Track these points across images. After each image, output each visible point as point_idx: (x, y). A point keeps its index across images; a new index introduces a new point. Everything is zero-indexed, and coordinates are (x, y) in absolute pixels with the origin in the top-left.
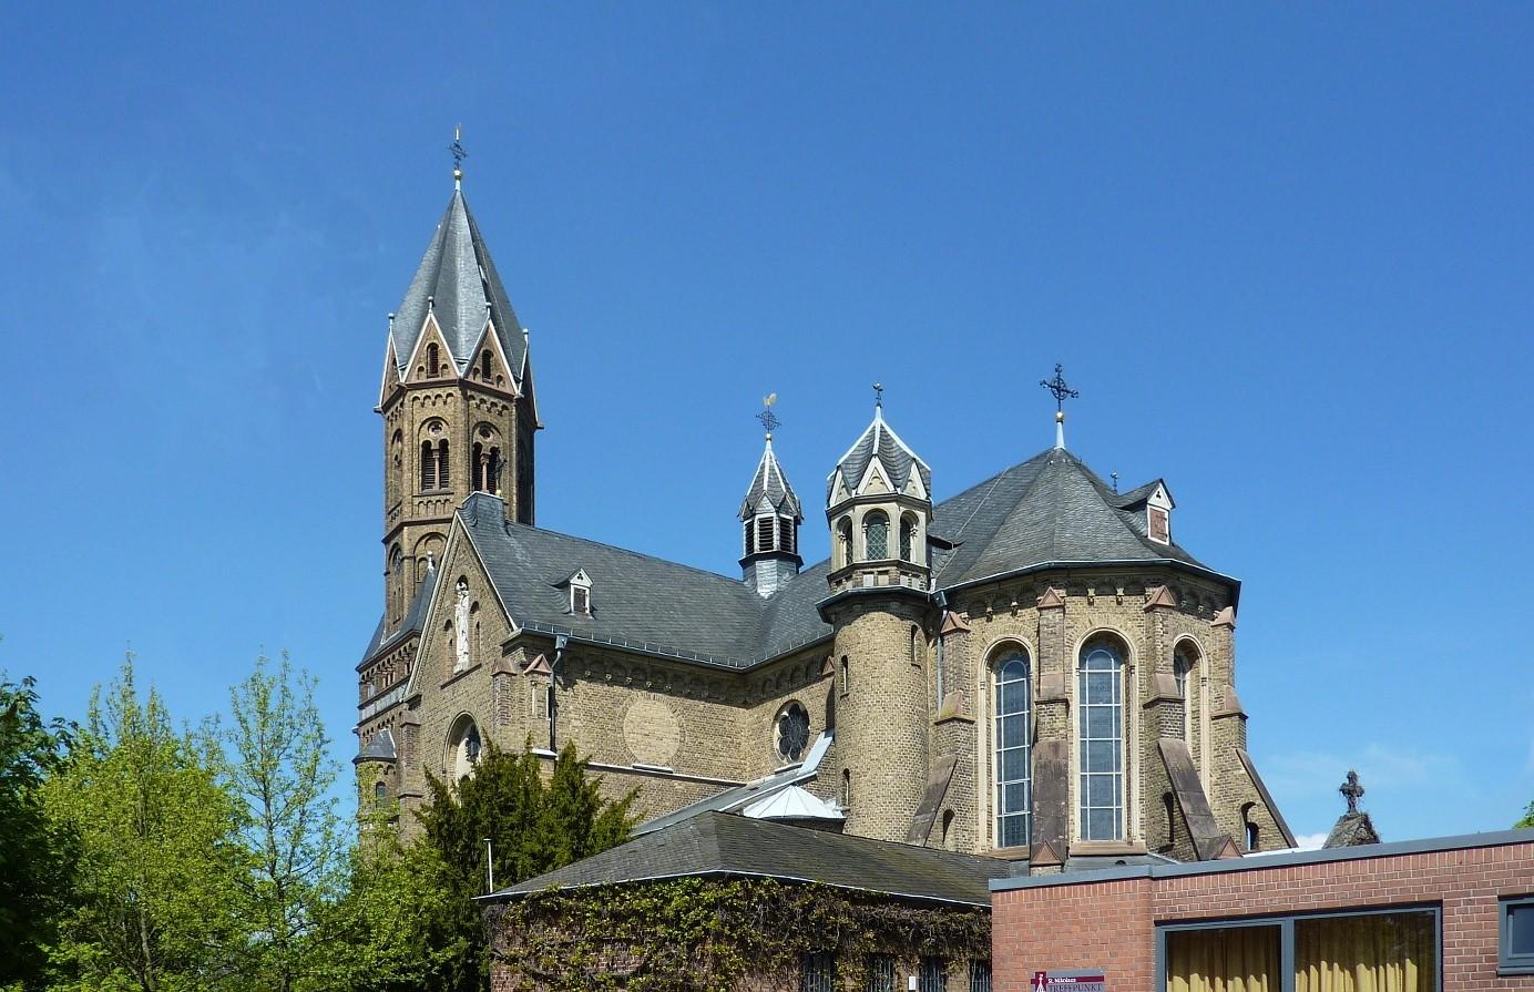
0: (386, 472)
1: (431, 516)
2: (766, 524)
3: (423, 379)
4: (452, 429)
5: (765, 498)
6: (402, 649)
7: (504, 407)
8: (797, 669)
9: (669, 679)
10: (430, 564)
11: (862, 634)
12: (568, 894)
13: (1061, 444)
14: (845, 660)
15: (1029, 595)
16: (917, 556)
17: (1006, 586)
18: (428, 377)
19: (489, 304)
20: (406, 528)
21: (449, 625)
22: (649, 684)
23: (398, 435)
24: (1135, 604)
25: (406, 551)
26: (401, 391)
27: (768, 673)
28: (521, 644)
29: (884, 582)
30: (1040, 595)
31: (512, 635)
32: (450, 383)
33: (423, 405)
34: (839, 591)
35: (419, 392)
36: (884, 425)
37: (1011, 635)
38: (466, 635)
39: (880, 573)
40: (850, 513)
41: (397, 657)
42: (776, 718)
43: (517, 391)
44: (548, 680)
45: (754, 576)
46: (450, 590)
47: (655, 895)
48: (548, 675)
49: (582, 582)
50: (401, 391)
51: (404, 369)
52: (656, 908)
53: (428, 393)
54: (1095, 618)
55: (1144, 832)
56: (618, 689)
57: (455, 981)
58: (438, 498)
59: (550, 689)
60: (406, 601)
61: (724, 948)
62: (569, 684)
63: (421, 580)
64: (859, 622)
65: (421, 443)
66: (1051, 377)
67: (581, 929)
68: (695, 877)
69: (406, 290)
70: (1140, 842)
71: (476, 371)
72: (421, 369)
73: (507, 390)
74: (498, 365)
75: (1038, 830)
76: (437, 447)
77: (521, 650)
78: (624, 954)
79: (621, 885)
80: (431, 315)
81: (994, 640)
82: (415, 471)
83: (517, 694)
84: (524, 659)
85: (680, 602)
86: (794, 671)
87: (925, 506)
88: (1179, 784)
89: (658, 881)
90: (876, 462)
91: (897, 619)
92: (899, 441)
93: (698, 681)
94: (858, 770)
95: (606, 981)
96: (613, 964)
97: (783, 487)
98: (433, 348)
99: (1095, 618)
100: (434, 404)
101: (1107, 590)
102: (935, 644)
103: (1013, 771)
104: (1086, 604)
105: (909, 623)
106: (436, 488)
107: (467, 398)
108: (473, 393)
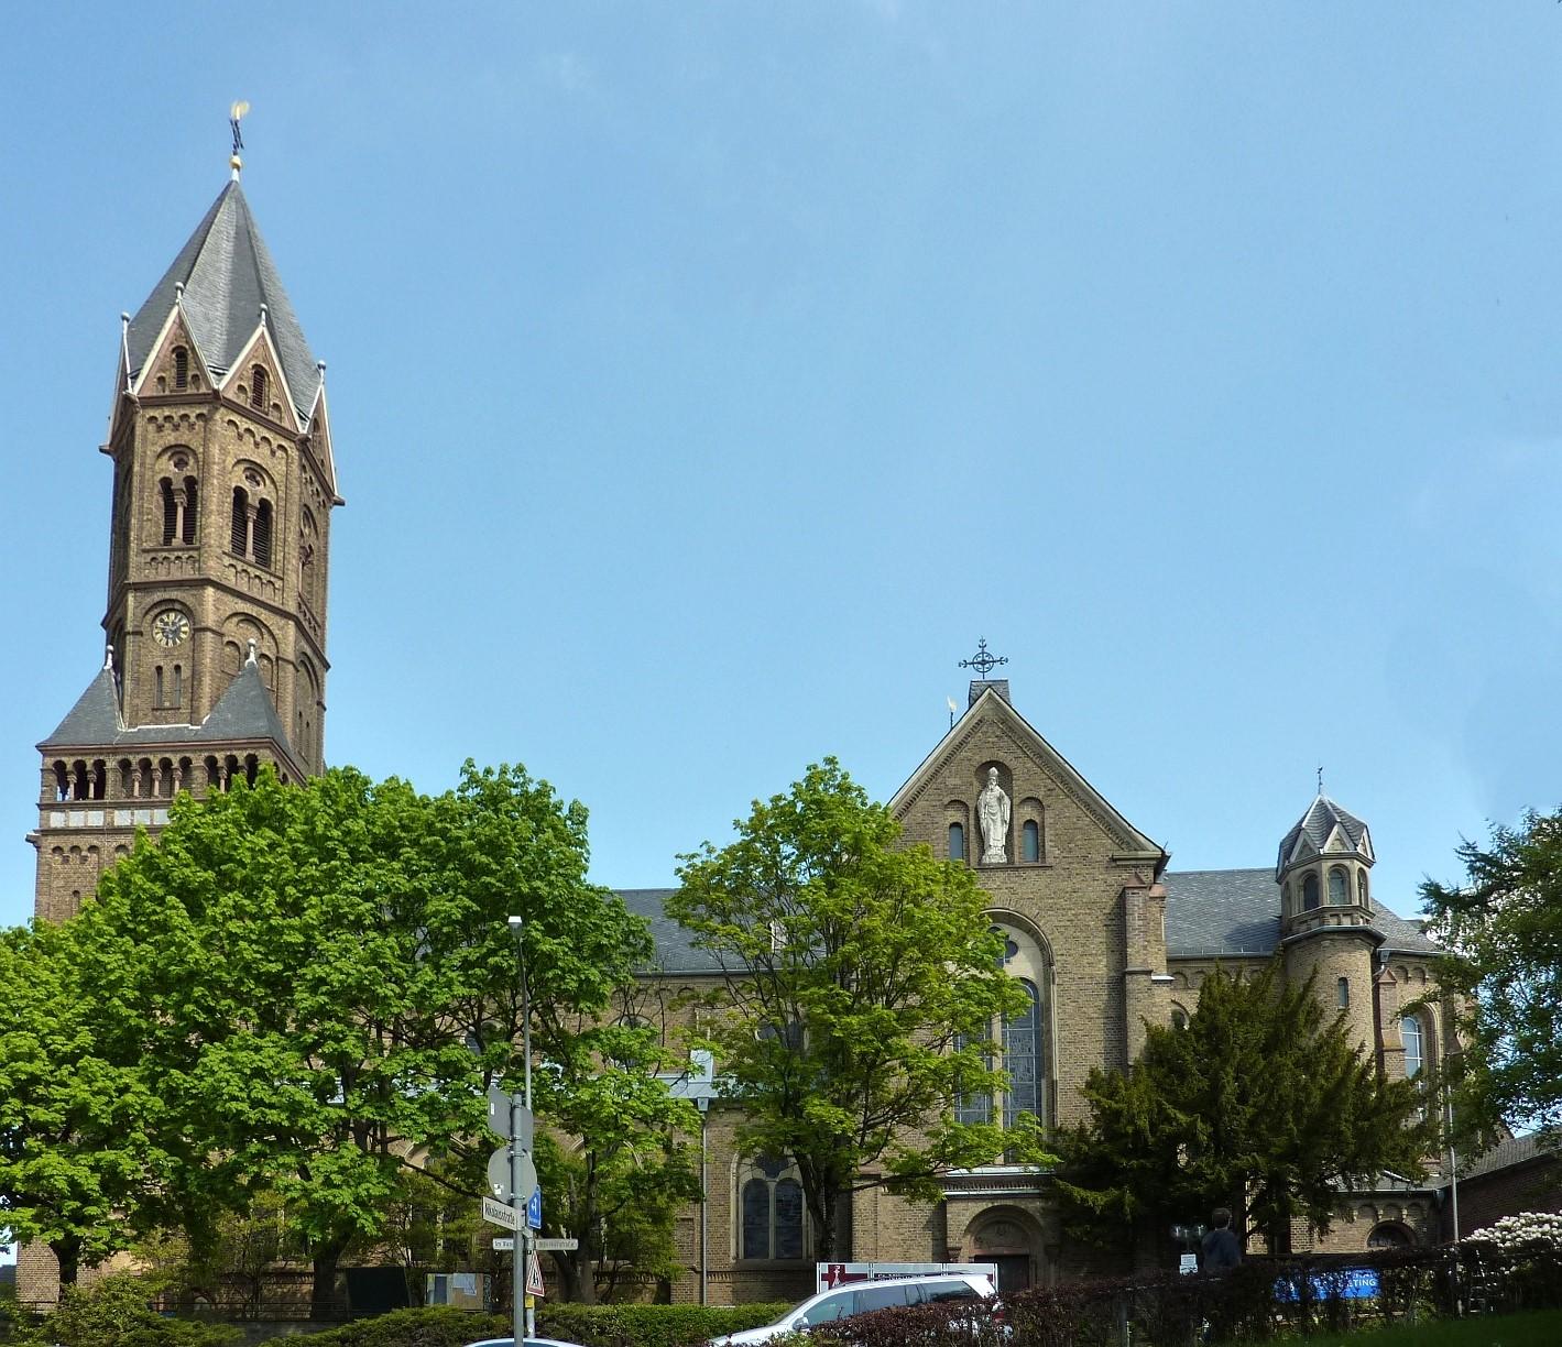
98: (260, 374)
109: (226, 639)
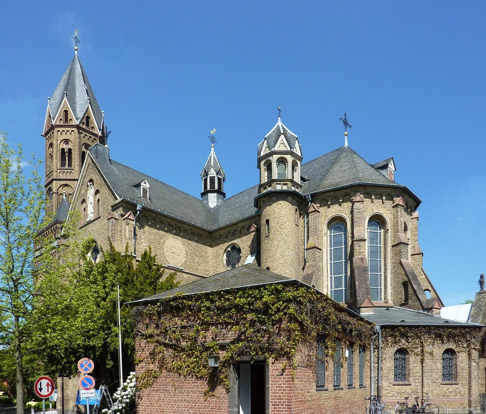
0: (46, 160)
1: (64, 177)
2: (212, 179)
3: (62, 123)
4: (73, 144)
5: (212, 168)
6: (52, 228)
7: (94, 139)
8: (236, 230)
9: (182, 231)
10: (64, 196)
11: (276, 210)
12: (189, 298)
13: (346, 144)
14: (268, 221)
15: (347, 197)
16: (297, 179)
17: (337, 193)
18: (64, 123)
19: (89, 98)
20: (54, 181)
21: (84, 201)
22: (174, 232)
23: (51, 145)
24: (389, 204)
25: (54, 190)
26: (53, 127)
27: (222, 232)
28: (121, 206)
29: (285, 188)
30: (352, 197)
31: (117, 202)
32: (73, 126)
33: (61, 134)
34: (265, 191)
35: (60, 128)
36: (282, 125)
37: (339, 213)
38: (92, 205)
39: (284, 184)
40: (271, 158)
41: (50, 232)
42: (225, 251)
43: (100, 134)
44: (134, 223)
45: (207, 199)
46: (85, 186)
47: (250, 296)
48: (133, 220)
49: (145, 185)
50: (53, 127)
51: (54, 119)
52: (249, 304)
53: (64, 129)
54: (374, 208)
55: (392, 298)
56: (161, 232)
57: (97, 354)
58: (67, 171)
59: (134, 227)
60: (54, 210)
61: (293, 326)
62: (141, 227)
63: (60, 202)
64: (274, 205)
65: (61, 149)
66: (343, 118)
67: (195, 318)
68: (278, 284)
69: (55, 88)
70: (390, 303)
71: (83, 123)
72: (61, 120)
73: (95, 132)
74: (92, 123)
75: (359, 293)
76: (67, 151)
77: (121, 209)
78: (224, 331)
79: (224, 291)
80: (65, 99)
81: (331, 216)
82: (58, 160)
83: (119, 228)
84: (123, 213)
85: (182, 203)
86: (235, 231)
87: (300, 159)
88: (411, 278)
89: (251, 288)
90: (282, 137)
91: (290, 205)
92: (289, 131)
93: (193, 233)
94: (273, 267)
95: (214, 346)
96: (216, 337)
97: (219, 165)
98: (66, 112)
99: (374, 208)
100: (66, 134)
101: (378, 197)
102: (304, 217)
103: (337, 271)
104: (370, 202)
105: (295, 207)
106: (67, 167)
107: (80, 133)
108: (82, 131)
109: (59, 194)
